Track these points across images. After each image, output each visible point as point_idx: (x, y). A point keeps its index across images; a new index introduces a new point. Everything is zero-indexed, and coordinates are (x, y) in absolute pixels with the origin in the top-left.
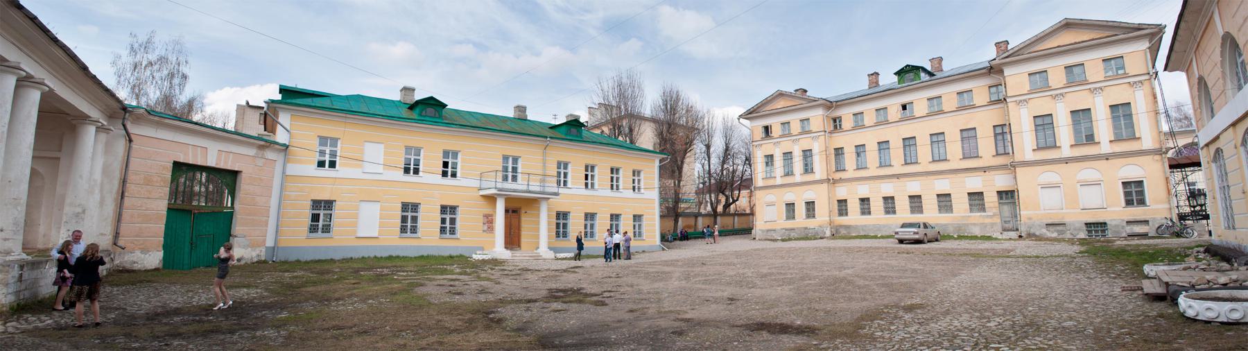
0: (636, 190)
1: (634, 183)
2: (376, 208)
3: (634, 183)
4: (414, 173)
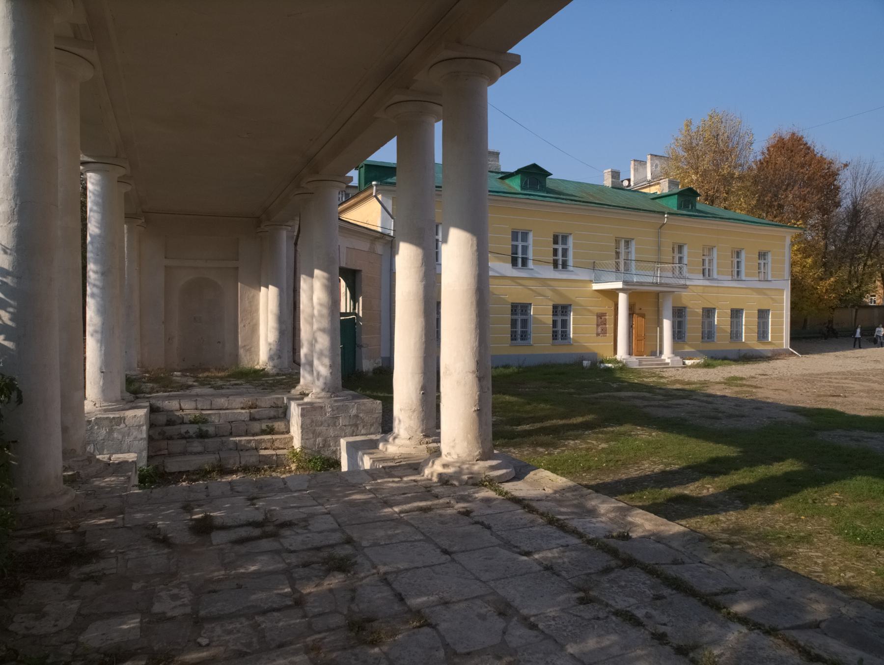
0: (560, 267)
1: (703, 264)
2: (343, 310)
3: (703, 264)
4: (563, 268)
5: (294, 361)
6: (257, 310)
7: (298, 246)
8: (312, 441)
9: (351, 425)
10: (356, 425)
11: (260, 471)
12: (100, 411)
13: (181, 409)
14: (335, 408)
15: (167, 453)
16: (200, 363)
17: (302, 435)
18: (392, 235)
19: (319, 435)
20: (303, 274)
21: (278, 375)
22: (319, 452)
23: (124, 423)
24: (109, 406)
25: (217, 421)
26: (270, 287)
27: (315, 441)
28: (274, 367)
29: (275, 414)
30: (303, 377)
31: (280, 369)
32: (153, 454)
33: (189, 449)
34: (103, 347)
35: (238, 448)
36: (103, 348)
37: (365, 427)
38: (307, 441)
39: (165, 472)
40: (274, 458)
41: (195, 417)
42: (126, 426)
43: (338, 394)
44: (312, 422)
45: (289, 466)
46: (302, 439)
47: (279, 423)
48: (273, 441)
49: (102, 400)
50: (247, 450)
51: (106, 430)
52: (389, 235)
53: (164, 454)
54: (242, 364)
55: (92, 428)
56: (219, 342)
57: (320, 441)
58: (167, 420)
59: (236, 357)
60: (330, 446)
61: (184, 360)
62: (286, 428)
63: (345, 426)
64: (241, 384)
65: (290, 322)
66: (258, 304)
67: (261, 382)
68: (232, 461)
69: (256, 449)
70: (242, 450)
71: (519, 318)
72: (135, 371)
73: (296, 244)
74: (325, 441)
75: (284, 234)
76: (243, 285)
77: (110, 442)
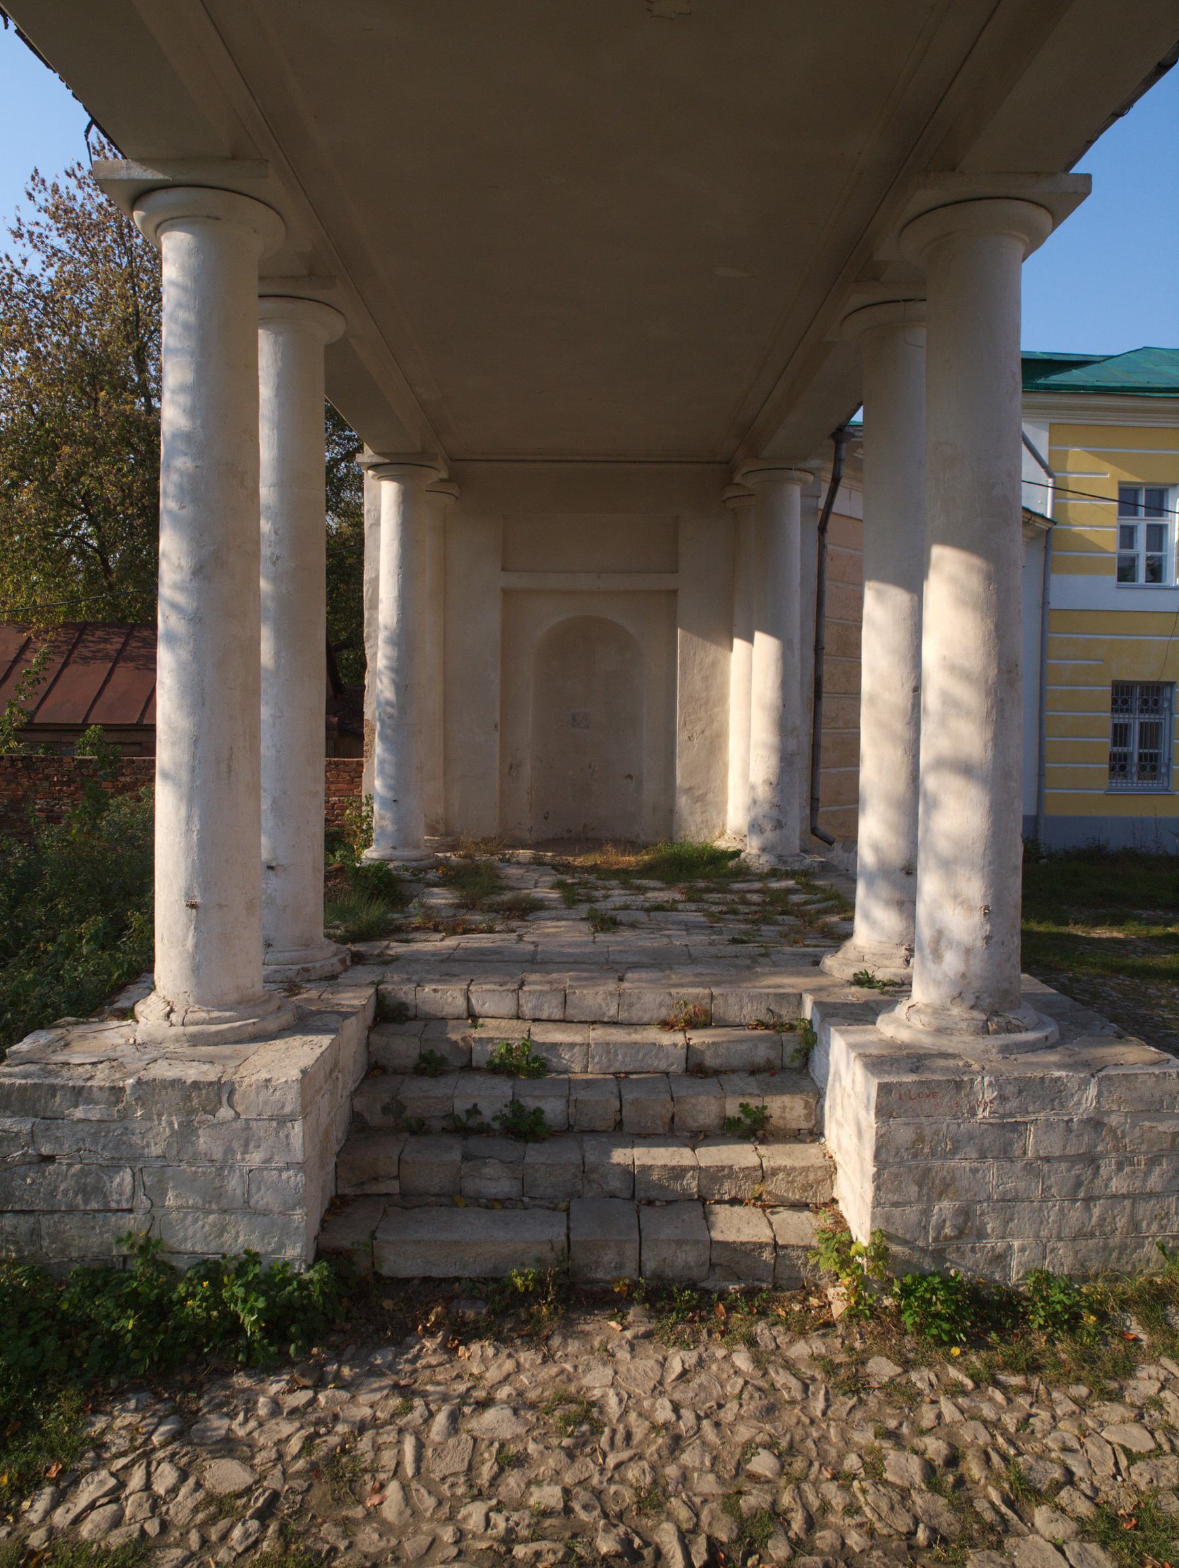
5: (814, 831)
6: (723, 699)
7: (829, 537)
8: (912, 1213)
9: (1073, 1160)
10: (1091, 1160)
11: (711, 1308)
12: (177, 1039)
13: (473, 1016)
14: (1010, 1090)
15: (397, 1191)
16: (585, 826)
17: (878, 1188)
18: (1049, 516)
19: (946, 1188)
20: (870, 579)
21: (774, 874)
22: (939, 1255)
23: (231, 1105)
24: (211, 1021)
25: (577, 1068)
26: (759, 636)
27: (927, 1213)
28: (764, 850)
29: (772, 1055)
30: (867, 916)
31: (780, 858)
32: (348, 1191)
33: (471, 1186)
34: (196, 819)
35: (640, 1194)
36: (196, 827)
37: (1127, 1169)
38: (897, 1212)
39: (378, 1276)
40: (767, 1255)
41: (509, 1050)
42: (238, 1115)
43: (1010, 1016)
44: (920, 1138)
45: (819, 1292)
46: (877, 1203)
47: (786, 1099)
48: (763, 1175)
49: (191, 1000)
50: (669, 1203)
51: (171, 1124)
52: (1043, 517)
53: (387, 1195)
54: (682, 833)
55: (125, 1115)
56: (630, 776)
57: (948, 1214)
58: (421, 1056)
59: (668, 814)
60: (981, 1235)
61: (546, 818)
62: (808, 1117)
63: (1047, 1159)
64: (670, 907)
65: (805, 729)
66: (725, 685)
67: (729, 897)
68: (609, 1257)
69: (702, 1200)
70: (650, 1203)
71: (1135, 721)
72: (417, 847)
73: (822, 529)
74: (965, 1214)
75: (795, 494)
76: (689, 635)
77: (184, 1166)
